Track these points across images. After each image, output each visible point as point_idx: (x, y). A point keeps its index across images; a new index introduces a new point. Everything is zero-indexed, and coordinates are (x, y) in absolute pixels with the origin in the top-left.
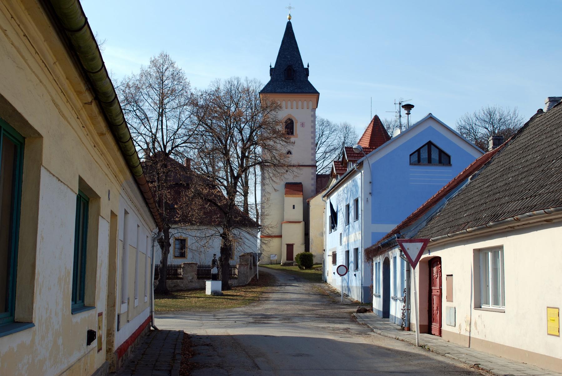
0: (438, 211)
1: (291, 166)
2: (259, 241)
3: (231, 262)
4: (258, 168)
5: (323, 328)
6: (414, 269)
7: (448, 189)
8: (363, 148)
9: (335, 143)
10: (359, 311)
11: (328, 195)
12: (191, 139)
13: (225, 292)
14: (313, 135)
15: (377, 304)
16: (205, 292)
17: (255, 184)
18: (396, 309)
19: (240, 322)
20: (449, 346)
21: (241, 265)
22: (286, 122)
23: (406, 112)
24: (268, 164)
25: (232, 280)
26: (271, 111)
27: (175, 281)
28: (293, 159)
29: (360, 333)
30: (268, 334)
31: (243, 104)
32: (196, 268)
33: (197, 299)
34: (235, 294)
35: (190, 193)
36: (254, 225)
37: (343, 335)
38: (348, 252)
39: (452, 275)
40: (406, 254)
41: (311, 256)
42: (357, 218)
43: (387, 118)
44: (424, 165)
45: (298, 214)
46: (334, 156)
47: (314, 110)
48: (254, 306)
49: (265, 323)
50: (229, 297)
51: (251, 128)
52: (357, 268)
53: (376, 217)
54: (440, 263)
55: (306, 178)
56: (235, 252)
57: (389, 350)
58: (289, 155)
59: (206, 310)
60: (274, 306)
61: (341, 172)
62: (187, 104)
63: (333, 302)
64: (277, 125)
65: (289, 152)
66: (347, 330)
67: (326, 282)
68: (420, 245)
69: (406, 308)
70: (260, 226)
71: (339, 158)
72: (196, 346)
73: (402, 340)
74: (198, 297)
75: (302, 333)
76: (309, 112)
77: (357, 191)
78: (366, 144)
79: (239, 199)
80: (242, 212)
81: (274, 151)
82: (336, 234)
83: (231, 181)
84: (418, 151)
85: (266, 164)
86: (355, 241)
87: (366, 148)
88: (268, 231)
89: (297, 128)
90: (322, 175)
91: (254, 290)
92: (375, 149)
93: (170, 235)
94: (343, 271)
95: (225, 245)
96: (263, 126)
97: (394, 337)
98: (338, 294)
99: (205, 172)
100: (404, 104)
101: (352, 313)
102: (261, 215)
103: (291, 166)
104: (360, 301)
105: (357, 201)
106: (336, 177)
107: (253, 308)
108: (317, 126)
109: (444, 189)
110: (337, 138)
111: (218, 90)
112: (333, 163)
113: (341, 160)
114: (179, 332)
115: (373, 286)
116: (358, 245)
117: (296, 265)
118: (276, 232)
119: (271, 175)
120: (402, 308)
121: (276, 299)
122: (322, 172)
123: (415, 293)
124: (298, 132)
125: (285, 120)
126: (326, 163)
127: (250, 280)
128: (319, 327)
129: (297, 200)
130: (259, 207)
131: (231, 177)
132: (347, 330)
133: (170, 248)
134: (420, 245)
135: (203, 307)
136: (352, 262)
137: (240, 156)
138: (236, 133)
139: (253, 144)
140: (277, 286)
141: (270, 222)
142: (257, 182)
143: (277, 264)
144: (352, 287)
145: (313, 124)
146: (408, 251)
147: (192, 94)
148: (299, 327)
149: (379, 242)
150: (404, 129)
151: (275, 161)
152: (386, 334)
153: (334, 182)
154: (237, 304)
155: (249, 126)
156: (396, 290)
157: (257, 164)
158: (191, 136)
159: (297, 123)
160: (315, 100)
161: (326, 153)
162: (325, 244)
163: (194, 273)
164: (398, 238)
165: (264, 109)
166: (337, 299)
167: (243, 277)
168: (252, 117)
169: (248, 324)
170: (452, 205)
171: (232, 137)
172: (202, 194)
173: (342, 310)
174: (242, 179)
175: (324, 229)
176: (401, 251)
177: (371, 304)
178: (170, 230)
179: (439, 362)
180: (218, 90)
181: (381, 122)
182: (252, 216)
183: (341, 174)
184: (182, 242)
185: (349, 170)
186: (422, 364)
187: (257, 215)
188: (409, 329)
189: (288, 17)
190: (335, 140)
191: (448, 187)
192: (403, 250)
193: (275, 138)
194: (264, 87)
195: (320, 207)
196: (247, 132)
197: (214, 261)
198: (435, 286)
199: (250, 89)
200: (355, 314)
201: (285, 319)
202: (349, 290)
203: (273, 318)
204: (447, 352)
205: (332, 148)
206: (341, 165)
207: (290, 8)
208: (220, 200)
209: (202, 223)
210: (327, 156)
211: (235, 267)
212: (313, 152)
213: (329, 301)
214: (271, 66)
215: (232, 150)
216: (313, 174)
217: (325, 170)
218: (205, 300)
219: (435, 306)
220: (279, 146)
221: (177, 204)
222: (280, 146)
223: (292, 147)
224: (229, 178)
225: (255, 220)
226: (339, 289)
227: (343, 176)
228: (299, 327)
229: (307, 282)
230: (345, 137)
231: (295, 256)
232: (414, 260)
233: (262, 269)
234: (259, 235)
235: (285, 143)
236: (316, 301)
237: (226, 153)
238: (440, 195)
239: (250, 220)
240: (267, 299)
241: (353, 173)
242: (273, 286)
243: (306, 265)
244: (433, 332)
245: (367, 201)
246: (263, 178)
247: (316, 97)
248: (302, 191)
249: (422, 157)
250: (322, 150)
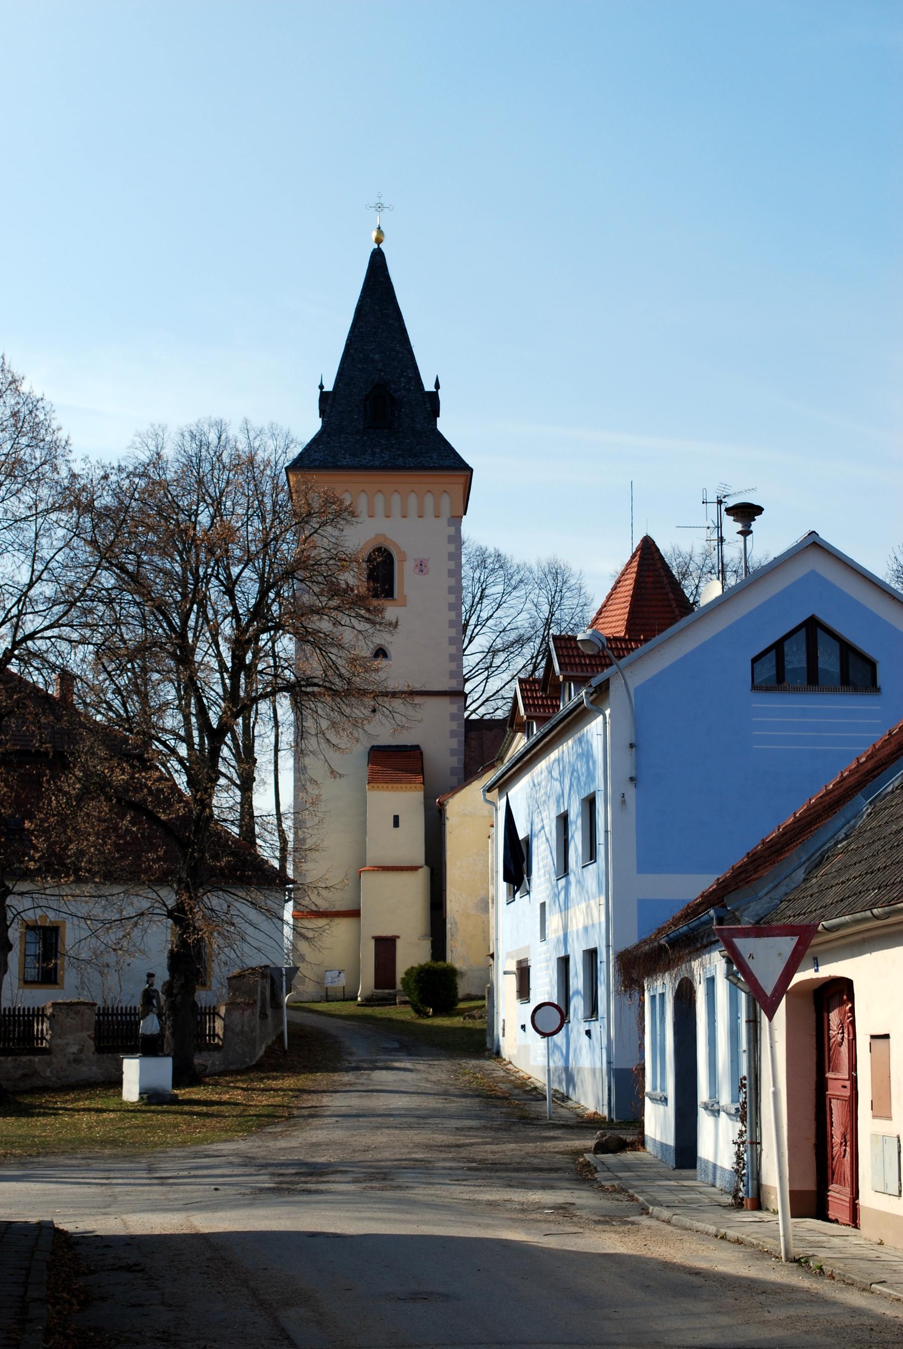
0: (842, 835)
1: (385, 694)
2: (287, 931)
3: (203, 997)
4: (284, 703)
5: (490, 1203)
6: (770, 1019)
7: (869, 765)
8: (608, 639)
9: (523, 621)
10: (601, 1148)
11: (503, 785)
12: (74, 613)
13: (183, 1093)
14: (452, 598)
15: (658, 1123)
16: (120, 1094)
17: (277, 750)
18: (717, 1141)
19: (232, 1191)
20: (884, 1257)
21: (231, 1006)
22: (370, 560)
23: (739, 526)
24: (316, 689)
25: (205, 1054)
26: (323, 524)
27: (25, 1059)
28: (395, 674)
29: (607, 1220)
30: (319, 1230)
31: (236, 507)
32: (90, 1018)
33: (94, 1117)
34: (215, 1097)
35: (72, 784)
36: (274, 881)
37: (554, 1228)
38: (564, 962)
39: (886, 1036)
40: (744, 969)
41: (451, 974)
42: (592, 855)
43: (680, 544)
44: (796, 690)
45: (410, 844)
46: (520, 662)
47: (456, 520)
48: (275, 1136)
49: (309, 1192)
50: (196, 1109)
51: (261, 578)
52: (593, 1011)
53: (650, 849)
54: (851, 999)
55: (432, 731)
56: (215, 965)
57: (697, 1273)
58: (381, 663)
59: (124, 1150)
60: (338, 1135)
61: (540, 713)
62: (60, 509)
63: (522, 1118)
64: (342, 569)
65: (381, 653)
66: (564, 1210)
67: (498, 1054)
68: (788, 944)
69: (746, 1137)
70: (293, 882)
71: (535, 669)
72: (93, 1272)
73: (739, 1242)
74: (99, 1111)
75: (426, 1223)
76: (442, 526)
77: (591, 776)
78: (616, 625)
79: (225, 800)
80: (236, 841)
81: (334, 650)
82: (525, 908)
83: (202, 744)
84: (778, 647)
85: (309, 689)
86: (586, 929)
87: (616, 639)
88: (315, 900)
89: (406, 577)
90: (481, 720)
91: (274, 1084)
92: (646, 640)
93: (10, 915)
94: (551, 1020)
95: (183, 943)
96: (300, 574)
97: (712, 1229)
98: (536, 1094)
99: (119, 715)
100: (731, 502)
101: (579, 1153)
102: (296, 850)
103: (385, 694)
104: (606, 1113)
105: (590, 803)
106: (525, 728)
107: (271, 1144)
108: (466, 571)
109: (860, 765)
110: (529, 605)
111: (157, 460)
112: (516, 685)
113: (540, 673)
114: (41, 1226)
115: (644, 1069)
116: (598, 941)
117: (405, 1003)
118: (339, 900)
119: (324, 724)
120: (736, 1138)
121: (344, 1111)
122: (481, 711)
123: (775, 1094)
125: (365, 555)
126: (494, 684)
127: (261, 1053)
128: (479, 1202)
129: (407, 801)
130: (287, 824)
131: (200, 730)
132: (564, 1210)
133: (10, 955)
134: (788, 944)
135: (114, 1143)
136: (577, 992)
137: (229, 665)
138: (214, 591)
139: (266, 630)
140: (348, 1070)
141: (324, 871)
142: (282, 746)
143: (345, 1000)
144: (579, 1070)
145: (452, 565)
146: (751, 964)
147: (74, 476)
148: (414, 1203)
149: (660, 931)
150: (732, 581)
151: (337, 680)
152: (687, 1221)
153: (520, 743)
154: (221, 1129)
155: (255, 571)
156: (715, 1079)
157: (282, 689)
158: (71, 600)
159: (402, 561)
160: (460, 489)
161: (493, 651)
162: (492, 936)
163: (85, 1034)
164: (721, 921)
165: (302, 519)
166: (535, 1107)
167: (243, 1044)
168: (266, 545)
169: (257, 1196)
170: (884, 816)
171: (202, 607)
172: (109, 784)
173: (548, 1144)
174: (234, 739)
175: (491, 890)
176: (729, 962)
177: (638, 1123)
178: (9, 900)
179: (855, 1311)
180: (157, 460)
181: (661, 558)
182: (267, 850)
183: (542, 720)
184: (48, 937)
185: (565, 706)
186: (799, 1318)
187: (283, 849)
188: (758, 1204)
189: (374, 234)
190: (521, 613)
191: (869, 758)
192: (734, 958)
193: (336, 608)
194: (299, 450)
195: (472, 815)
196: (249, 590)
197: (148, 996)
198: (836, 1069)
199: (258, 458)
200: (588, 1157)
201: (371, 1177)
202: (570, 1079)
203: (335, 1172)
204: (877, 1278)
205: (513, 636)
206: (540, 691)
207: (380, 207)
208: (167, 804)
209: (109, 877)
210: (497, 661)
211: (215, 1013)
212: (453, 649)
213: (509, 1115)
214: (321, 387)
215: (203, 646)
216: (453, 717)
217: (492, 704)
218: (121, 1120)
219: (837, 1132)
220: (348, 636)
221: (31, 817)
222: (353, 634)
223: (387, 636)
224: (195, 733)
225: (276, 864)
226: (539, 1079)
227: (548, 726)
228: (414, 1203)
229: (437, 1056)
230: (552, 605)
231: (400, 974)
232: (769, 991)
233: (300, 1017)
234: (288, 912)
235: (368, 626)
236: (468, 1117)
237: (184, 656)
238: (846, 784)
239: (260, 864)
240: (315, 1114)
241: (578, 717)
242: (335, 1070)
243: (435, 1003)
244: (832, 1214)
245: (624, 802)
246: (300, 733)
247: (462, 480)
248: (420, 771)
249: (788, 667)
250: (481, 642)
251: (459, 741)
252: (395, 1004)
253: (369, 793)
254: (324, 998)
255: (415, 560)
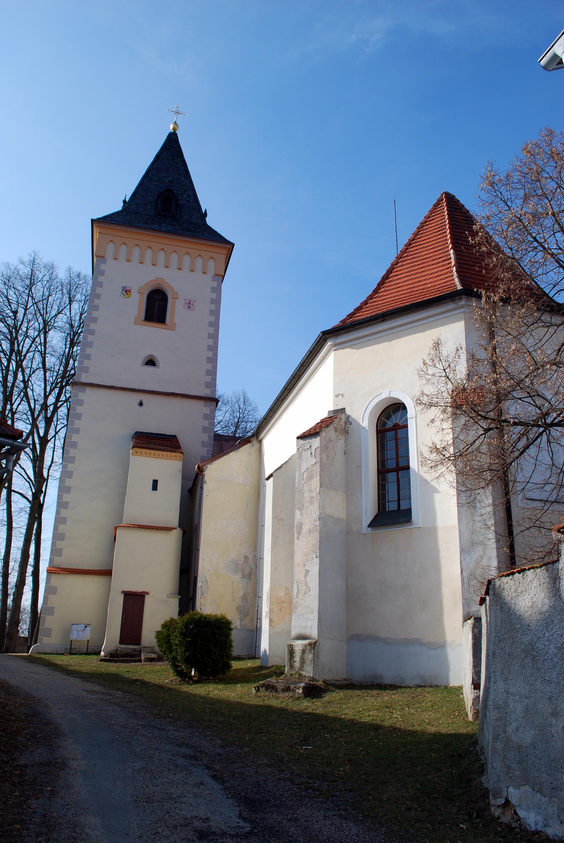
16: (194, 607)
45: (166, 506)
76: (208, 281)
124: (177, 319)
129: (166, 468)
143: (87, 654)
160: (223, 258)
247: (225, 252)
251: (209, 436)
252: (140, 661)
253: (132, 458)
254: (68, 651)
255: (185, 300)
